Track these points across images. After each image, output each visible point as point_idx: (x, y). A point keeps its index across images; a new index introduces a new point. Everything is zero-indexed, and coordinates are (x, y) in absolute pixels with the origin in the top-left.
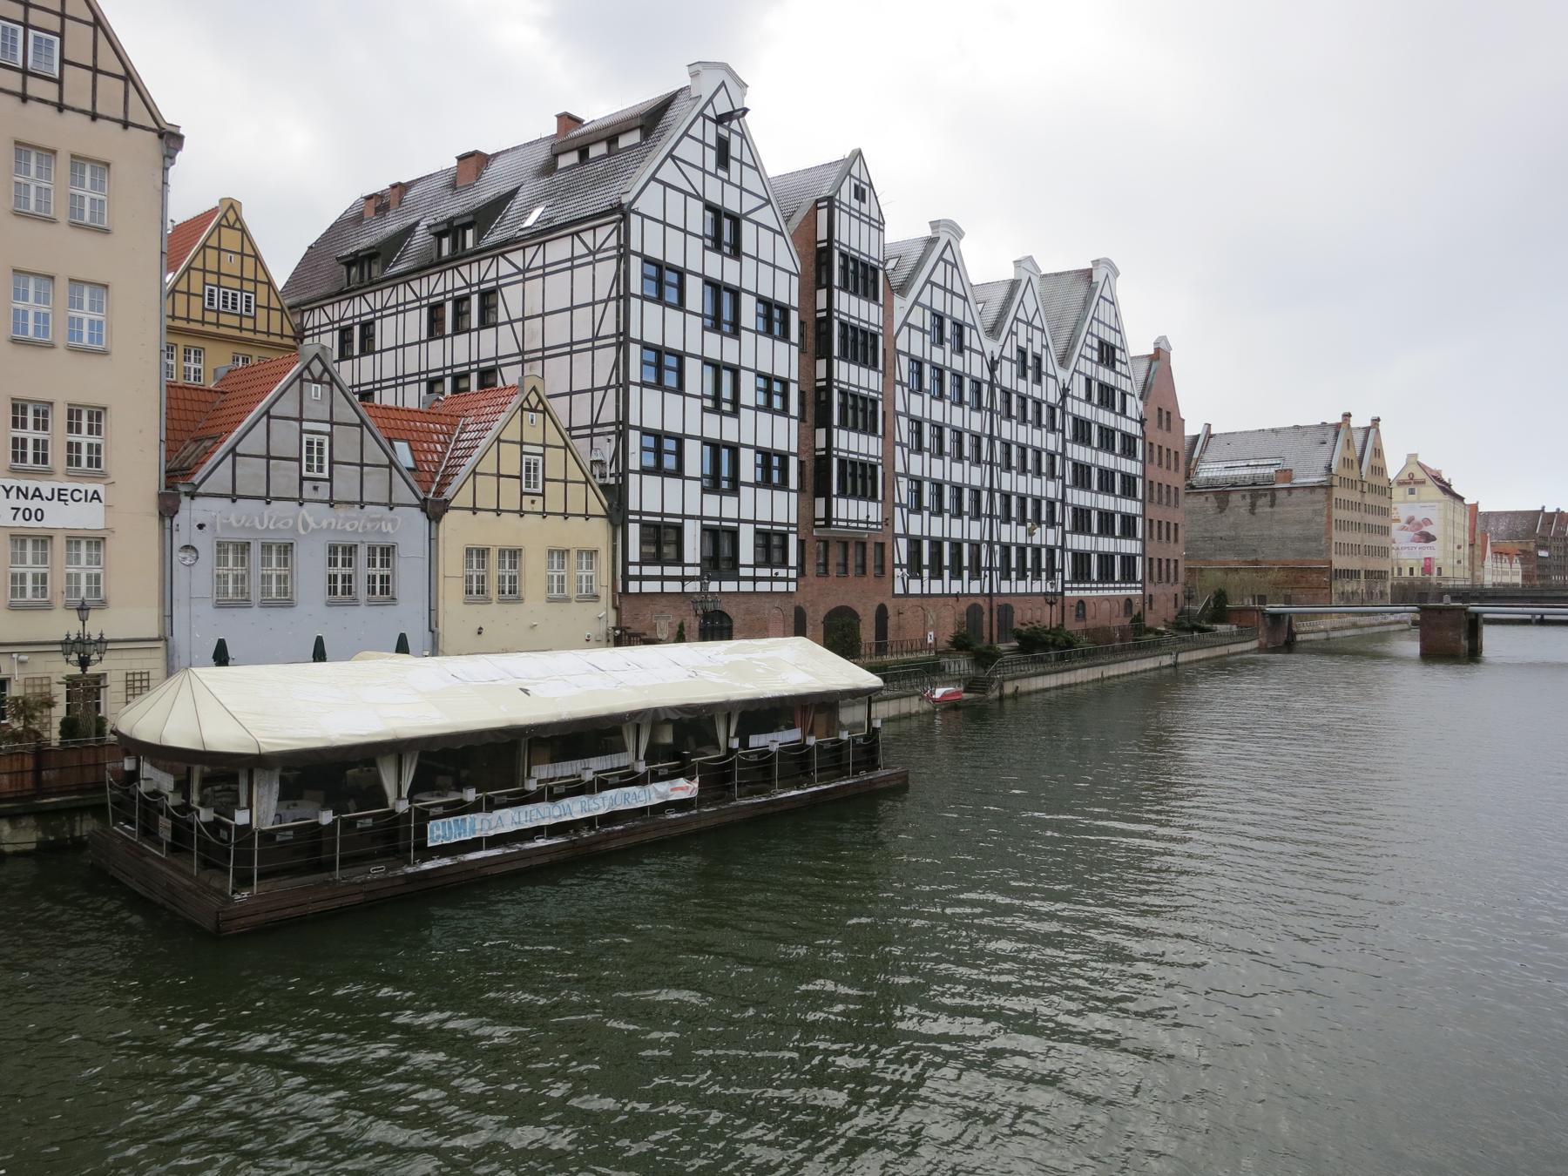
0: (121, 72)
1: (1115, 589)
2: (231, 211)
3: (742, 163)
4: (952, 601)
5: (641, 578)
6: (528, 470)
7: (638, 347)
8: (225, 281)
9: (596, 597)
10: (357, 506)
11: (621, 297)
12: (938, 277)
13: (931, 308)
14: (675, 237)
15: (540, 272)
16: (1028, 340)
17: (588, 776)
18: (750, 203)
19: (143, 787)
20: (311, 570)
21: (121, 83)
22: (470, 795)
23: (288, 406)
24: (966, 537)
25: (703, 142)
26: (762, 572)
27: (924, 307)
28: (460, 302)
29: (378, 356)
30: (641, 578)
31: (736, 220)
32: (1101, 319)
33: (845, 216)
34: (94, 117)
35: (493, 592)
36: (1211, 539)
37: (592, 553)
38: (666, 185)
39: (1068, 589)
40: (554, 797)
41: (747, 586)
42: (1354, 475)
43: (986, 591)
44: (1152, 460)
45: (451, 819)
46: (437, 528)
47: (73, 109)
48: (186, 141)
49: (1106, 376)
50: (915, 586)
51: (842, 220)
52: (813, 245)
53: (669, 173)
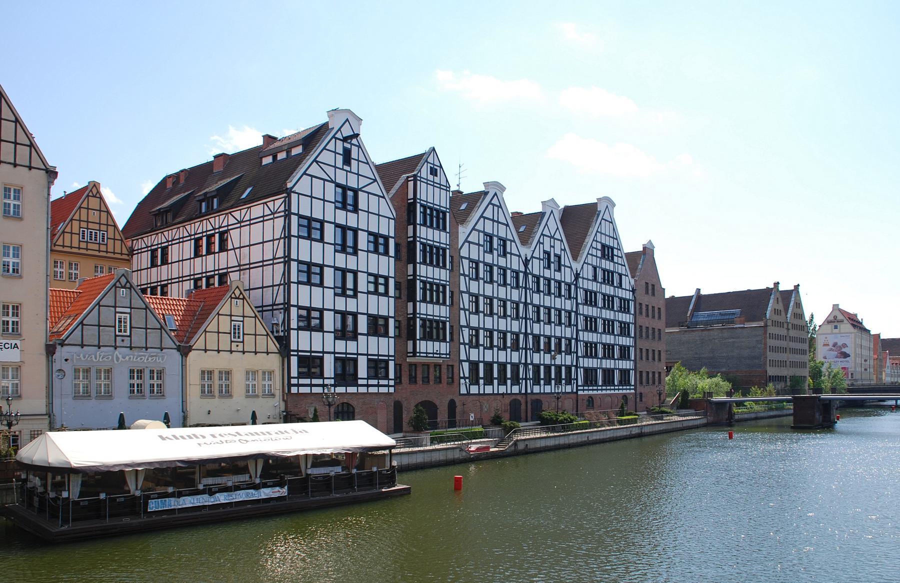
0: (28, 143)
1: (614, 389)
2: (94, 188)
3: (358, 161)
4: (499, 397)
5: (298, 385)
6: (235, 329)
7: (296, 263)
8: (91, 226)
9: (273, 395)
10: (144, 349)
11: (286, 237)
12: (488, 214)
13: (484, 232)
14: (318, 204)
15: (248, 223)
16: (551, 246)
17: (230, 484)
18: (363, 182)
19: (29, 485)
20: (121, 381)
21: (28, 148)
22: (170, 490)
23: (110, 300)
24: (495, 360)
25: (335, 153)
26: (371, 382)
27: (479, 231)
28: (209, 237)
29: (170, 265)
30: (298, 385)
31: (356, 192)
32: (603, 232)
33: (424, 185)
34: (15, 165)
35: (217, 393)
36: (699, 358)
37: (271, 373)
38: (312, 176)
39: (581, 390)
40: (211, 493)
41: (363, 390)
42: (781, 319)
43: (523, 391)
44: (641, 313)
45: (159, 500)
46: (186, 360)
47: (5, 163)
48: (59, 173)
49: (607, 265)
50: (474, 390)
51: (422, 188)
52: (406, 201)
53: (315, 170)
